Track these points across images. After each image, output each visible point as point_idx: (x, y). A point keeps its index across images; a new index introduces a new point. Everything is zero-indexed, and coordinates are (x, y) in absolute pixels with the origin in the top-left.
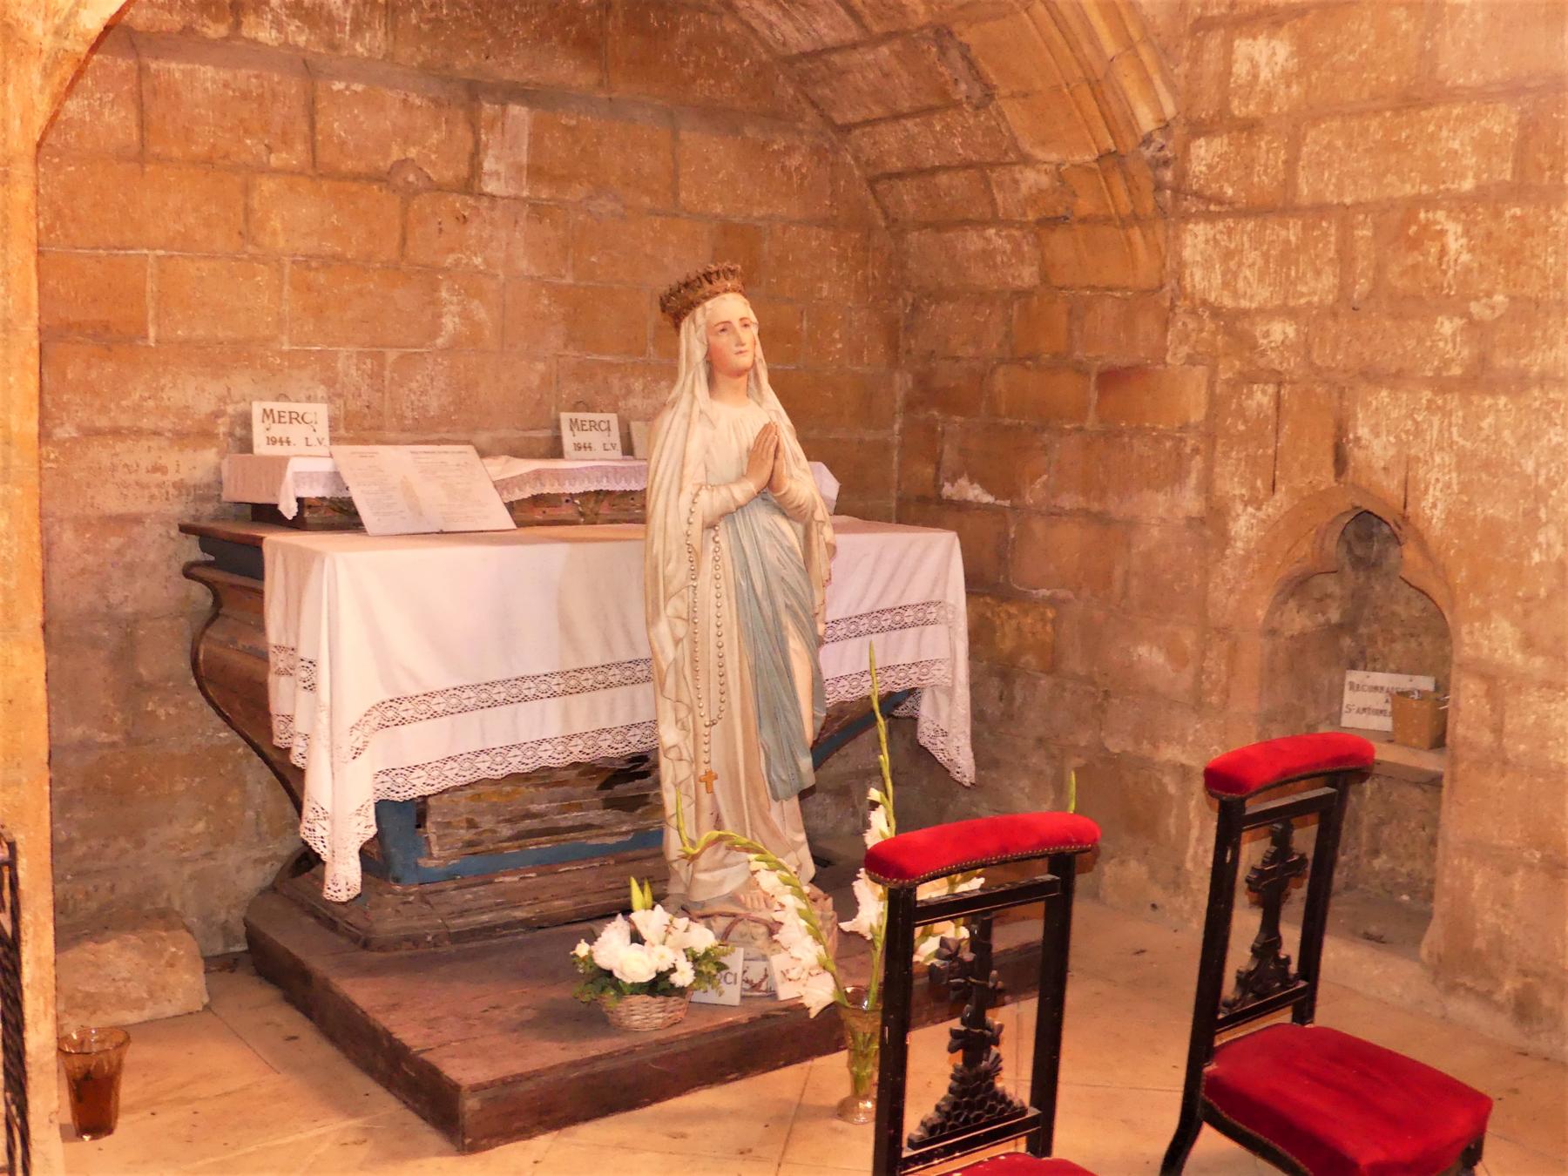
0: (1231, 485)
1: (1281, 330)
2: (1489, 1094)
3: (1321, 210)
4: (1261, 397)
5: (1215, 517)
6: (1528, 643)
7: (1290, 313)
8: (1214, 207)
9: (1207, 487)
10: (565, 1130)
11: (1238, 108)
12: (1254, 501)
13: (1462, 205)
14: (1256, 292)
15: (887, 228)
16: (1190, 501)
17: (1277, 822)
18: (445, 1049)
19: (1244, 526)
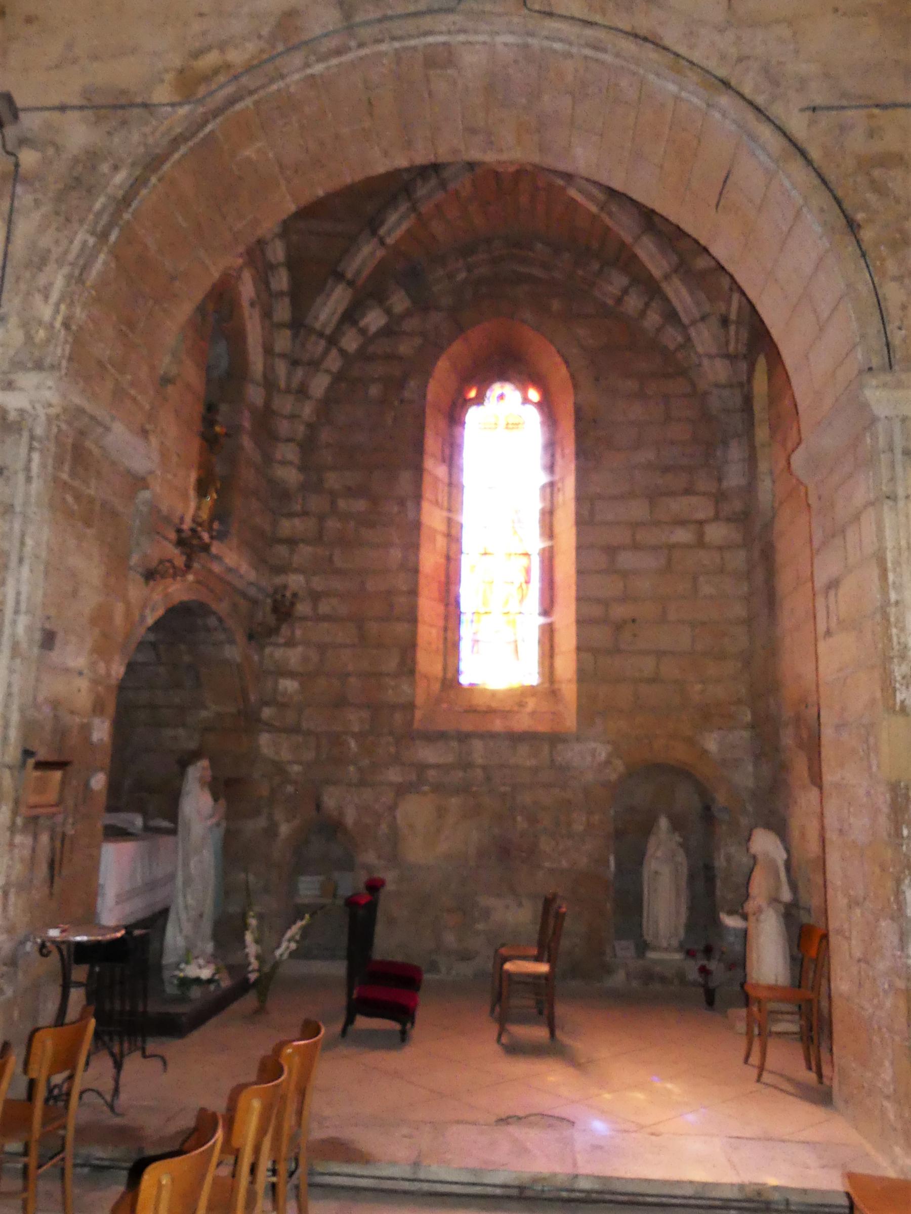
0: (279, 815)
1: (296, 768)
2: (416, 963)
3: (309, 733)
4: (290, 789)
5: (271, 831)
6: (379, 857)
7: (300, 763)
8: (270, 727)
9: (270, 817)
10: (831, 953)
11: (280, 699)
12: (288, 821)
13: (354, 735)
14: (285, 755)
15: (59, 357)
16: (261, 822)
17: (674, 82)
18: (896, 940)
19: (284, 829)
